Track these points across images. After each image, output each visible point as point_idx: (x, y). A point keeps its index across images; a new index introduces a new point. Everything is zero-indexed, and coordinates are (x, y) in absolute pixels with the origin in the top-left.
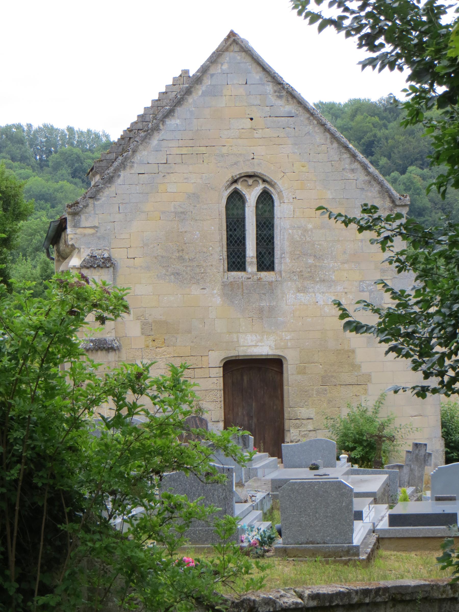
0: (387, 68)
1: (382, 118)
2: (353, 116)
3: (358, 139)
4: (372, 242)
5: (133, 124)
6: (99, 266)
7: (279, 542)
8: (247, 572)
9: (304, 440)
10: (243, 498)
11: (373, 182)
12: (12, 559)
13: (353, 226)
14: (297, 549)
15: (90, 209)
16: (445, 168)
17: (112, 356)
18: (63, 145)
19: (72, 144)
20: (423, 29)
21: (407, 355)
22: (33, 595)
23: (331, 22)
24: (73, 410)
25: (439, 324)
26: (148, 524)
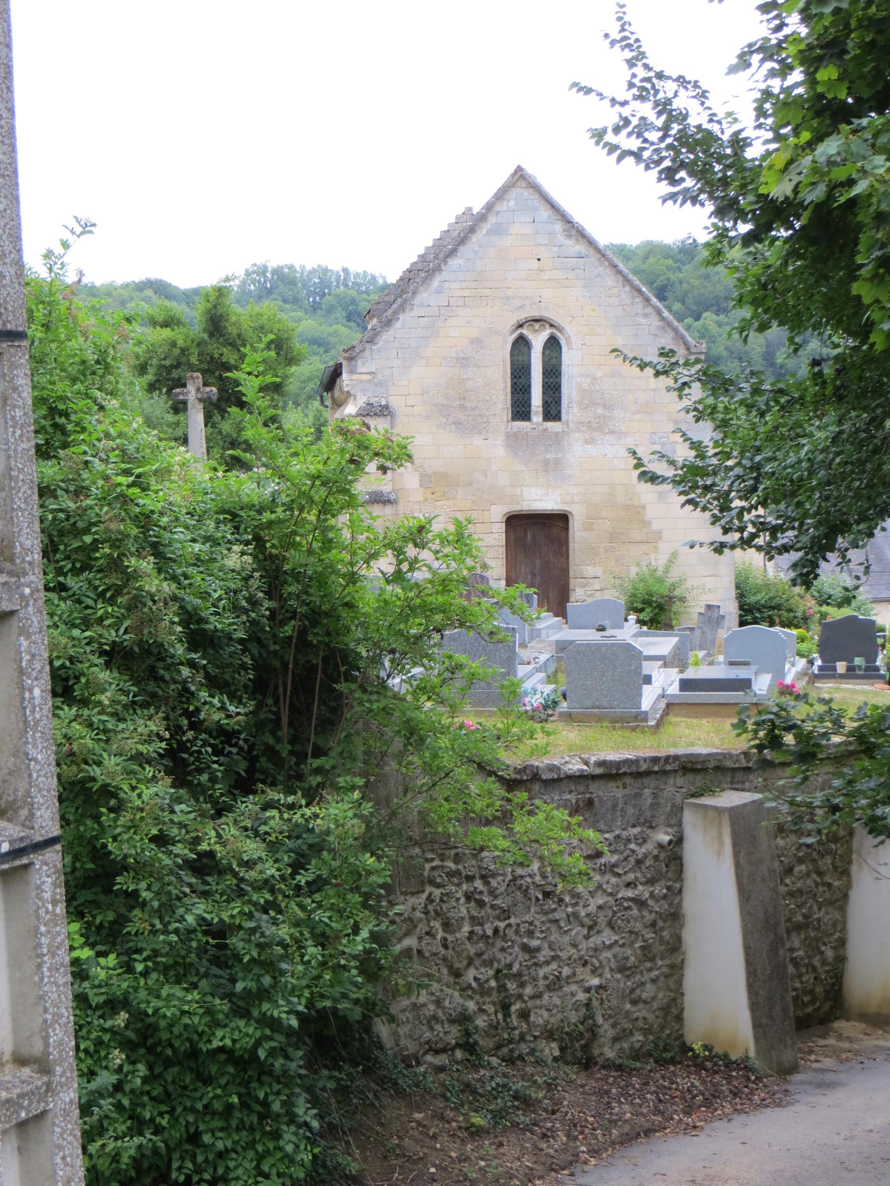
0: (689, 203)
1: (676, 261)
2: (646, 258)
3: (650, 283)
4: (668, 389)
5: (413, 264)
6: (375, 414)
7: (564, 706)
8: (531, 738)
9: (590, 600)
10: (526, 660)
11: (667, 328)
12: (285, 720)
13: (649, 371)
14: (582, 714)
15: (367, 354)
16: (746, 312)
17: (388, 510)
18: (338, 286)
19: (346, 286)
20: (728, 162)
21: (704, 509)
22: (306, 757)
23: (630, 153)
24: (352, 564)
25: (738, 477)
26: (428, 685)
